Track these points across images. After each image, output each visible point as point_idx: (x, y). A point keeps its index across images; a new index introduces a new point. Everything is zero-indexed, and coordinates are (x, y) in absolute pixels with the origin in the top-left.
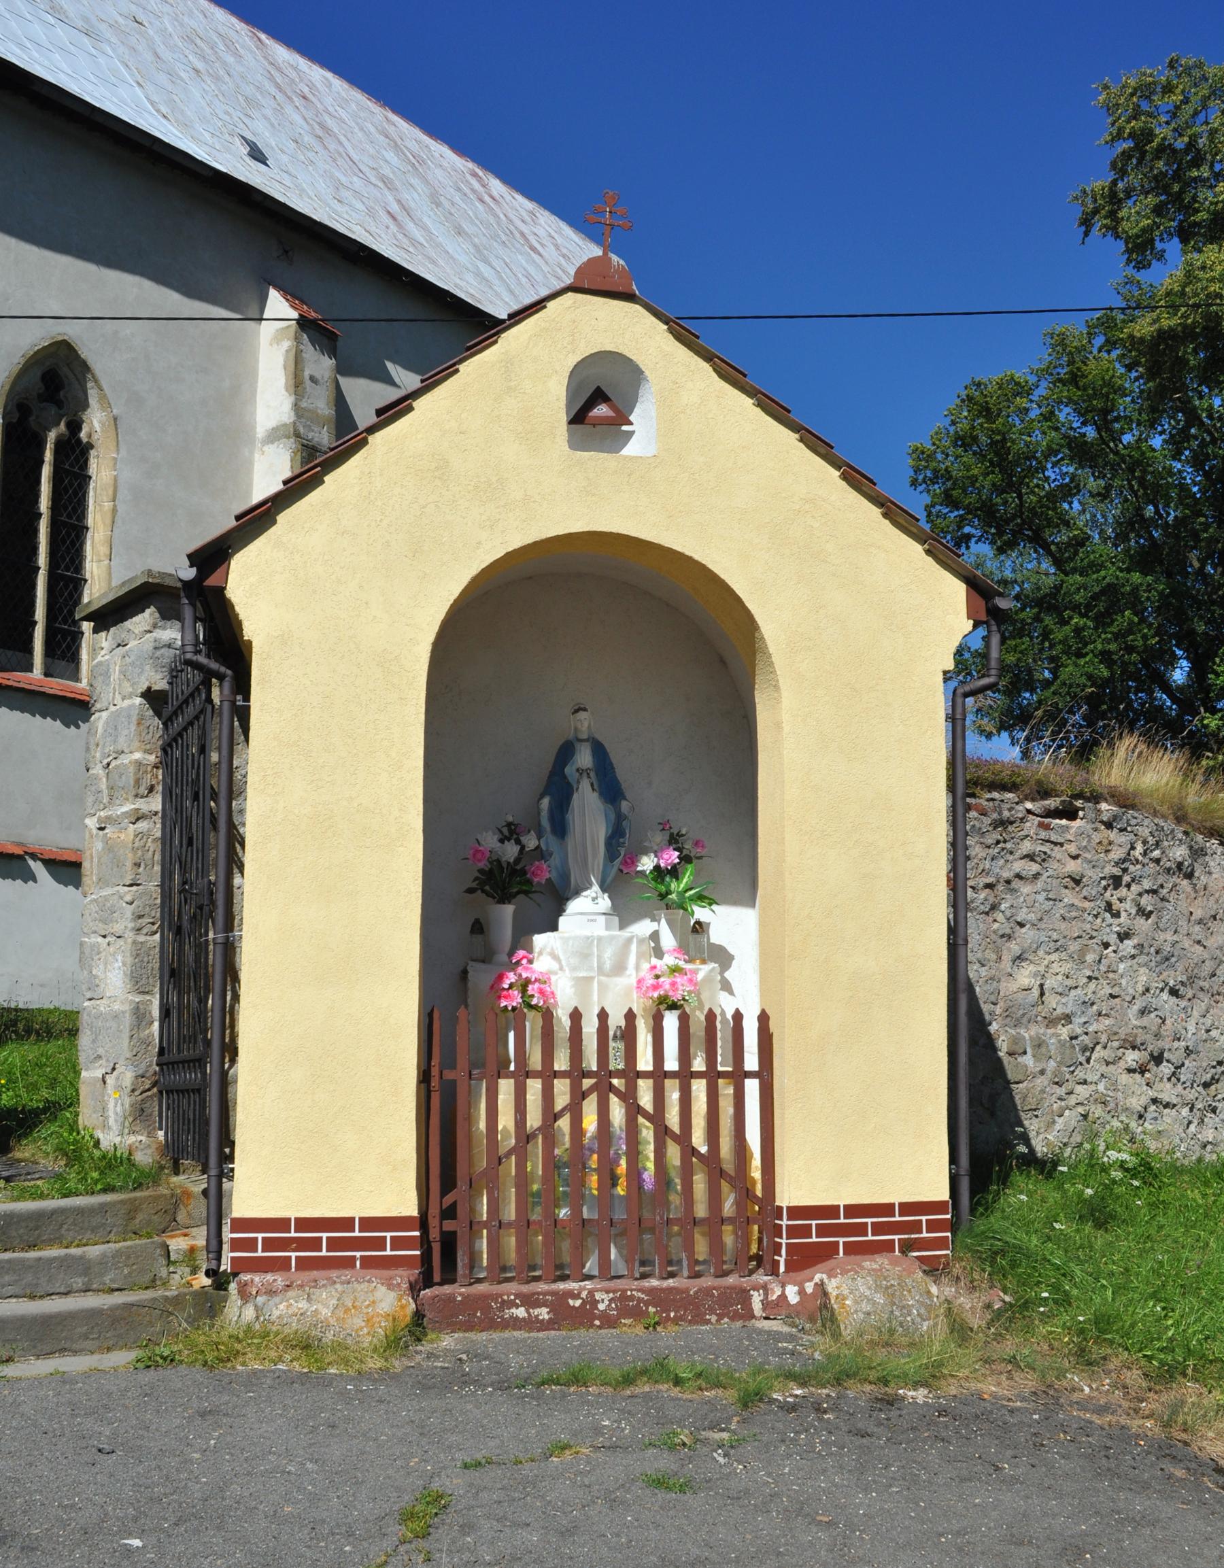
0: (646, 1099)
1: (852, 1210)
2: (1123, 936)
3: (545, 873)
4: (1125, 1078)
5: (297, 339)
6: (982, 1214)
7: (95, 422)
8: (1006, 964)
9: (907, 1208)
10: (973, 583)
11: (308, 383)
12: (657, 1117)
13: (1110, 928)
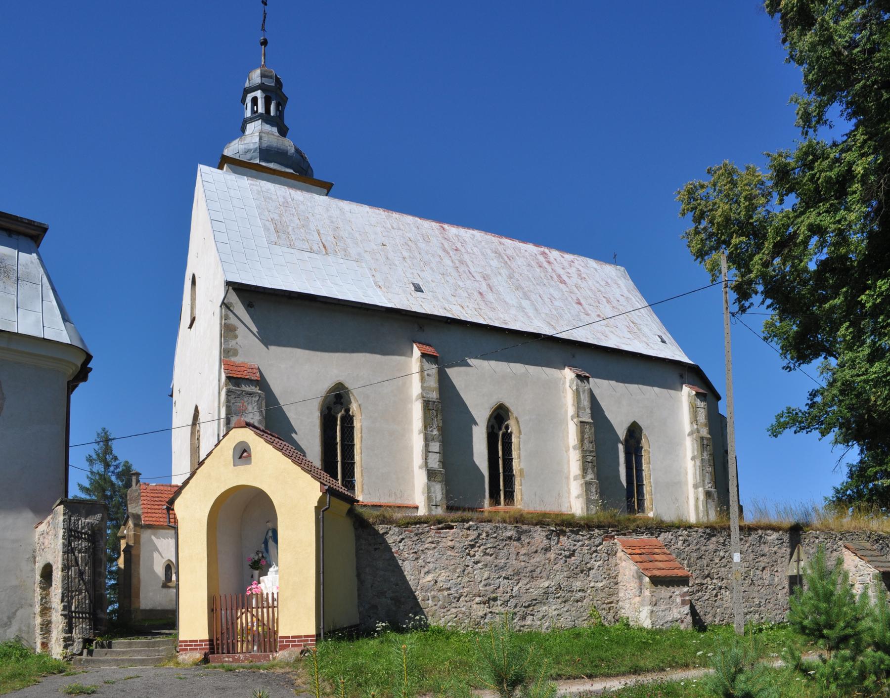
0: (254, 613)
1: (293, 637)
2: (476, 563)
3: (263, 563)
4: (475, 606)
5: (421, 362)
6: (682, 681)
7: (354, 407)
8: (422, 575)
9: (305, 636)
10: (321, 483)
11: (426, 377)
12: (257, 617)
13: (470, 561)
